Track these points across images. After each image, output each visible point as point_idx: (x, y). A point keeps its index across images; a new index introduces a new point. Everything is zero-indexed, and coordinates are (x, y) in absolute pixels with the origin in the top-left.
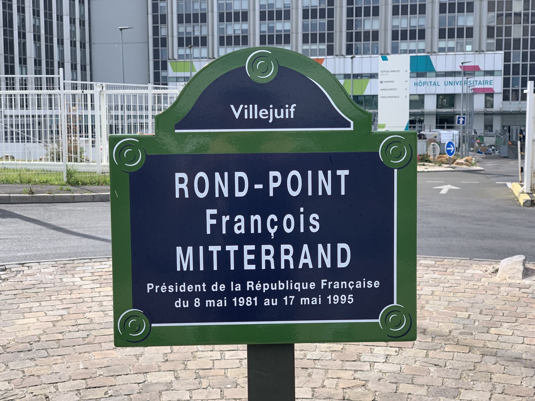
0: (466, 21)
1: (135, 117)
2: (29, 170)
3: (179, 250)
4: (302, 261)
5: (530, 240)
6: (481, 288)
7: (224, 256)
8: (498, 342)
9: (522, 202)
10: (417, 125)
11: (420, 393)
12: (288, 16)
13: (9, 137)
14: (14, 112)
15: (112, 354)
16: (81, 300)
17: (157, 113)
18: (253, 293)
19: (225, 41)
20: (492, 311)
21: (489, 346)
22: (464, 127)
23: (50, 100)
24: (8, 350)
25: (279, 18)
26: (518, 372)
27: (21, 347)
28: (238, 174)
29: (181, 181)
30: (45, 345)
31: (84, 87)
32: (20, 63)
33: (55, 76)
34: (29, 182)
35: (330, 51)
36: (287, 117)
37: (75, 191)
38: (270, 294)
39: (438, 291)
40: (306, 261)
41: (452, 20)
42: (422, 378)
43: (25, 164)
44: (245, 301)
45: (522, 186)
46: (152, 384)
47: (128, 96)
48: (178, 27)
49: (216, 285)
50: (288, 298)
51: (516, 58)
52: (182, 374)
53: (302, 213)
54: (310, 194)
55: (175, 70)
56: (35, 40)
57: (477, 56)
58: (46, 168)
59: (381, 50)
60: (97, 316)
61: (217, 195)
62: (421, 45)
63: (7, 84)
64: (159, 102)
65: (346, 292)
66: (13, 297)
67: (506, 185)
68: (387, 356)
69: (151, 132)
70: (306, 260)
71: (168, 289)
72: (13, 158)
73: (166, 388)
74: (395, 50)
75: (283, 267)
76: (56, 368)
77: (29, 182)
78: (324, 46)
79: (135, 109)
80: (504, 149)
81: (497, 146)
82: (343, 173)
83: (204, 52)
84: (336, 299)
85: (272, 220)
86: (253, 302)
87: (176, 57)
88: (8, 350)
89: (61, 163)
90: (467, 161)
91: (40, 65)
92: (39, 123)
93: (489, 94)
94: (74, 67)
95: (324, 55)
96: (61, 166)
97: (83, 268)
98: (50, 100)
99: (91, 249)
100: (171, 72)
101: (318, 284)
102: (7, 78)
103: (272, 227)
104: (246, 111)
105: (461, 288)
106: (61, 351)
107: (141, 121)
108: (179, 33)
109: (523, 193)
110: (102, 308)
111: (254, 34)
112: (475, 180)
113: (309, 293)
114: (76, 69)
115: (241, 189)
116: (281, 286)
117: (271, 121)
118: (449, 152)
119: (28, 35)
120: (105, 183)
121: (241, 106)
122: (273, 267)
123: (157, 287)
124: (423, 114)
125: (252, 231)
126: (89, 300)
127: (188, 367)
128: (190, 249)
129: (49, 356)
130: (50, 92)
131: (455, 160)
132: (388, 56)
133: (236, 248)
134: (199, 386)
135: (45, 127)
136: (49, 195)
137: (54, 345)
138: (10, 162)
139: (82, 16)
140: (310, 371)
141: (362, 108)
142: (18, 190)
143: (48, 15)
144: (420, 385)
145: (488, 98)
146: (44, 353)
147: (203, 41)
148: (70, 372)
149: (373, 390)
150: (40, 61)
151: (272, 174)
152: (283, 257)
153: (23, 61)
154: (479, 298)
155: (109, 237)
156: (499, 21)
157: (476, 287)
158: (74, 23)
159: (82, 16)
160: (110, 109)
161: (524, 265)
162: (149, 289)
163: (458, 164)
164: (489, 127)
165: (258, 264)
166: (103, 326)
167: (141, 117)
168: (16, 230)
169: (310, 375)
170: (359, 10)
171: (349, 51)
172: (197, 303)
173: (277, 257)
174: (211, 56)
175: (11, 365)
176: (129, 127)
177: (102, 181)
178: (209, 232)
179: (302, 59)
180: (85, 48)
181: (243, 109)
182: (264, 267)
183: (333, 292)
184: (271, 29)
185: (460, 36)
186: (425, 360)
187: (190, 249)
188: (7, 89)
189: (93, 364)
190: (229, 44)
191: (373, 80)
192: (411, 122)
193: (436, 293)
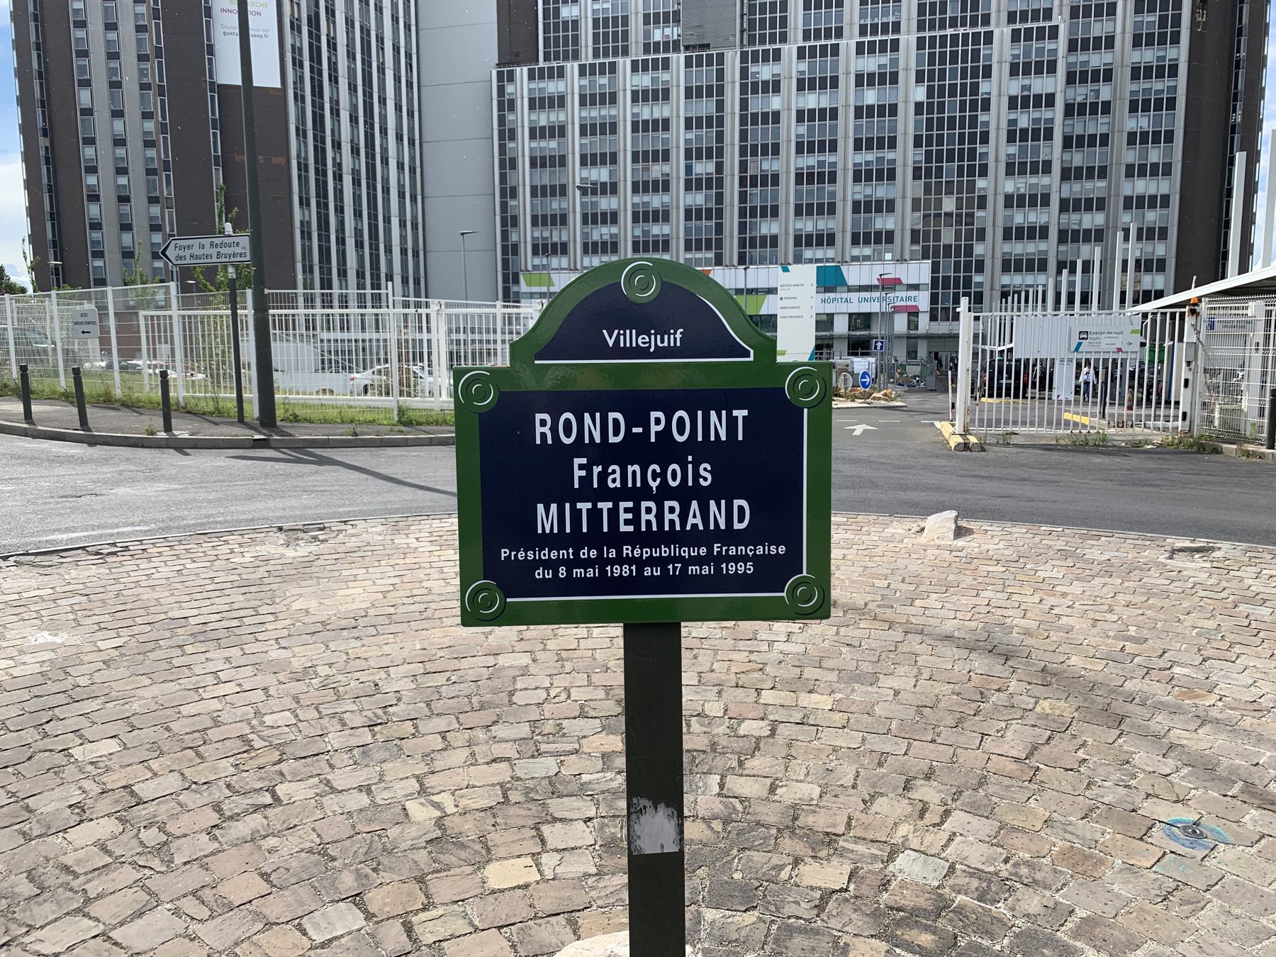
0: (885, 223)
1: (481, 341)
2: (351, 407)
3: (540, 507)
4: (691, 521)
5: (963, 492)
6: (904, 550)
7: (595, 514)
8: (924, 617)
9: (953, 445)
10: (825, 351)
11: (829, 678)
12: (666, 218)
13: (326, 365)
14: (332, 336)
15: (456, 631)
16: (417, 566)
17: (515, 338)
18: (630, 561)
19: (591, 248)
20: (917, 579)
21: (914, 621)
22: (882, 354)
23: (377, 321)
24: (328, 627)
25: (656, 220)
26: (949, 653)
27: (344, 623)
28: (612, 415)
29: (543, 423)
30: (373, 621)
31: (418, 305)
32: (339, 275)
33: (383, 291)
34: (352, 422)
35: (719, 261)
36: (672, 344)
37: (409, 433)
38: (652, 562)
39: (851, 554)
40: (695, 521)
41: (868, 222)
42: (831, 660)
43: (347, 400)
44: (621, 570)
45: (953, 425)
46: (504, 668)
47: (472, 316)
48: (532, 232)
49: (586, 551)
50: (673, 567)
51: (946, 268)
52: (541, 656)
53: (690, 462)
54: (700, 439)
55: (529, 284)
56: (356, 246)
57: (899, 266)
58: (372, 404)
59: (781, 259)
60: (436, 586)
61: (587, 441)
62: (830, 253)
63: (323, 302)
64: (510, 323)
65: (745, 558)
66: (334, 562)
67: (933, 424)
68: (790, 634)
69: (502, 360)
70: (695, 520)
71: (526, 556)
72: (332, 392)
73: (521, 673)
74: (798, 259)
75: (667, 528)
76: (387, 649)
77: (352, 422)
78: (711, 255)
79: (480, 333)
80: (931, 380)
81: (922, 377)
82: (740, 414)
83: (564, 262)
84: (732, 568)
85: (654, 471)
86: (631, 571)
87: (530, 268)
88: (328, 627)
89: (391, 398)
90: (885, 395)
91: (364, 277)
92: (364, 349)
93: (913, 313)
94: (405, 280)
95: (711, 265)
96: (391, 402)
97: (419, 527)
98: (377, 321)
99: (429, 504)
100: (524, 287)
101: (710, 550)
102: (323, 294)
103: (654, 480)
104: (622, 337)
105: (878, 551)
106: (393, 628)
107: (488, 347)
108: (533, 238)
109: (954, 434)
110: (443, 576)
111: (626, 240)
112: (896, 418)
113: (699, 561)
114: (407, 283)
115: (616, 433)
116: (665, 551)
117: (652, 350)
118: (864, 384)
119: (388, 101)
120: (445, 423)
121: (616, 331)
122: (655, 528)
123: (513, 553)
124: (832, 338)
125: (630, 485)
126: (427, 565)
127: (548, 647)
128: (554, 507)
129: (378, 634)
130: (376, 311)
131: (871, 394)
132: (789, 267)
133: (610, 505)
134: (561, 671)
135: (371, 354)
136: (297, 224)
137: (385, 620)
138: (327, 396)
139: (414, 217)
140: (695, 651)
141: (759, 329)
142: (338, 431)
143: (373, 217)
144: (830, 670)
145: (912, 318)
146: (372, 631)
147: (563, 249)
148: (405, 654)
149: (773, 675)
150: (363, 274)
151: (654, 415)
152: (668, 516)
153: (343, 273)
154: (901, 563)
155: (455, 490)
156: (926, 223)
157: (898, 550)
158: (405, 226)
159: (414, 217)
160: (450, 331)
161: (956, 522)
162: (503, 555)
163: (874, 398)
164: (912, 354)
165: (637, 526)
166: (444, 598)
167: (488, 342)
168: (337, 481)
169: (695, 657)
170: (753, 209)
171: (742, 260)
172: (562, 572)
173: (660, 517)
174: (572, 267)
175: (332, 646)
176: (473, 354)
177: (441, 420)
178: (576, 486)
179: (686, 270)
180: (418, 257)
181: (619, 334)
182: (643, 529)
183: (728, 559)
184: (646, 233)
185: (878, 241)
186: (836, 638)
187: (554, 507)
188: (324, 307)
189: (432, 644)
190: (595, 252)
191: (770, 296)
192: (818, 347)
193: (849, 557)
